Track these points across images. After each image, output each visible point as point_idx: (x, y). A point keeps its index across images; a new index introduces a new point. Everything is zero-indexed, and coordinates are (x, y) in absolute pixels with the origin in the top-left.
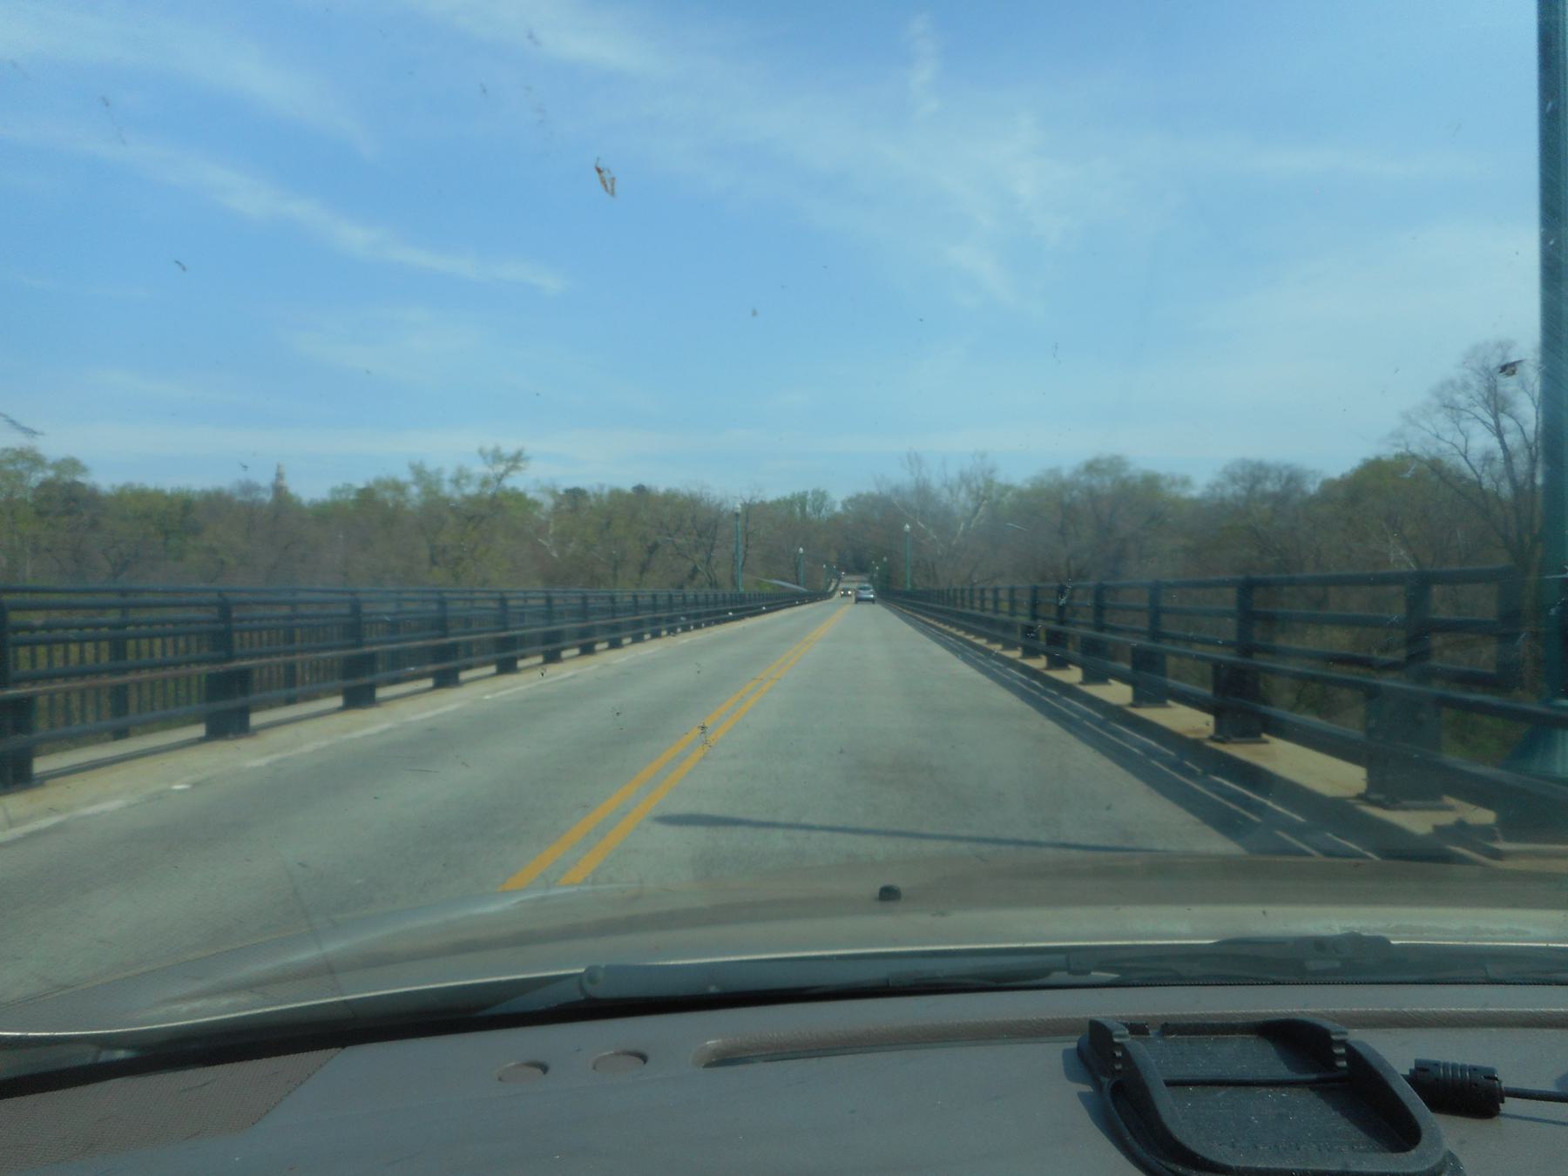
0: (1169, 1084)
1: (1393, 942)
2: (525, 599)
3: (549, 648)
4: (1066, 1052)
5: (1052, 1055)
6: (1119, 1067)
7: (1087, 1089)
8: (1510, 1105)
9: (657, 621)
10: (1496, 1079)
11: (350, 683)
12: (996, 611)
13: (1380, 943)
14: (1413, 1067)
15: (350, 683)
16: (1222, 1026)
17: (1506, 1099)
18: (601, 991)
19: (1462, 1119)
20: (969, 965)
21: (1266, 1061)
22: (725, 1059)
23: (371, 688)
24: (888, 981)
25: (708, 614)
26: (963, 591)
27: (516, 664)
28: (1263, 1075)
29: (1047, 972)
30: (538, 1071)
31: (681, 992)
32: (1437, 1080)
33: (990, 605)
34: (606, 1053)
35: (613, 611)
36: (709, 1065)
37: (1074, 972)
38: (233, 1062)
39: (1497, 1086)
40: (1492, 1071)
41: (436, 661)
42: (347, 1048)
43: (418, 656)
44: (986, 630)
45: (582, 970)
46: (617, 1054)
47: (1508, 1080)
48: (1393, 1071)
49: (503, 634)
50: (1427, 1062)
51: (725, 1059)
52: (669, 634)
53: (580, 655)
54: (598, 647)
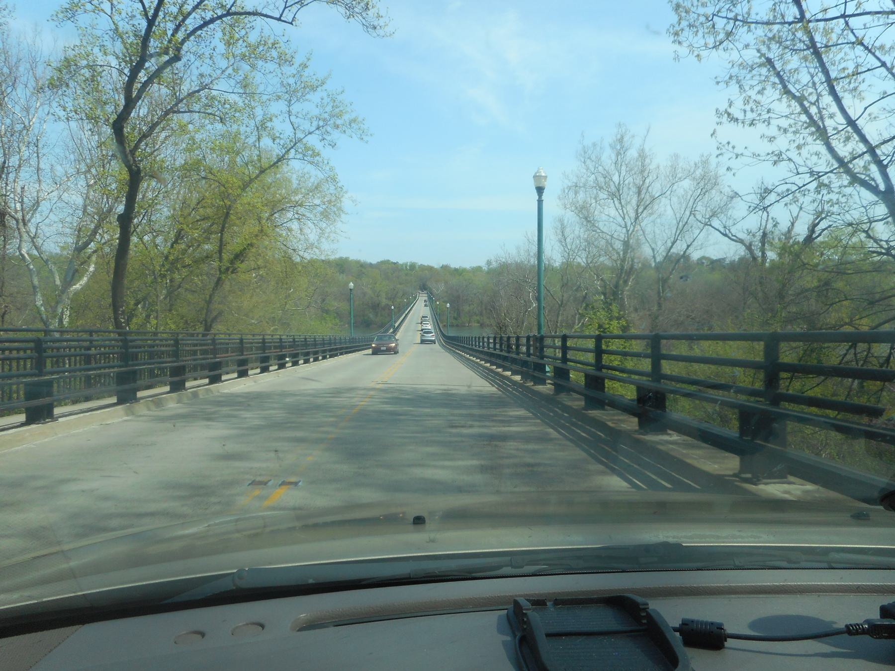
0: (548, 635)
1: (684, 545)
2: (254, 335)
3: (264, 365)
4: (500, 617)
5: (492, 619)
6: (644, 621)
7: (509, 638)
8: (730, 643)
9: (316, 353)
10: (723, 629)
11: (212, 373)
12: (495, 349)
13: (678, 546)
14: (681, 623)
15: (212, 373)
16: (573, 600)
17: (728, 639)
18: (244, 584)
19: (708, 651)
20: (453, 565)
21: (606, 619)
22: (312, 625)
23: (220, 376)
24: (410, 574)
25: (331, 350)
26: (475, 338)
27: (184, 385)
28: (604, 628)
29: (499, 567)
30: (199, 636)
31: (285, 583)
32: (692, 630)
33: (491, 346)
34: (240, 624)
35: (281, 347)
36: (300, 630)
37: (513, 567)
38: (7, 637)
39: (723, 633)
40: (722, 624)
41: (210, 371)
42: (85, 625)
43: (203, 367)
44: (299, 398)
45: (235, 571)
46: (247, 624)
47: (730, 629)
48: (668, 625)
49: (241, 357)
50: (688, 620)
51: (312, 625)
52: (305, 363)
53: (28, 422)
54: (271, 368)
